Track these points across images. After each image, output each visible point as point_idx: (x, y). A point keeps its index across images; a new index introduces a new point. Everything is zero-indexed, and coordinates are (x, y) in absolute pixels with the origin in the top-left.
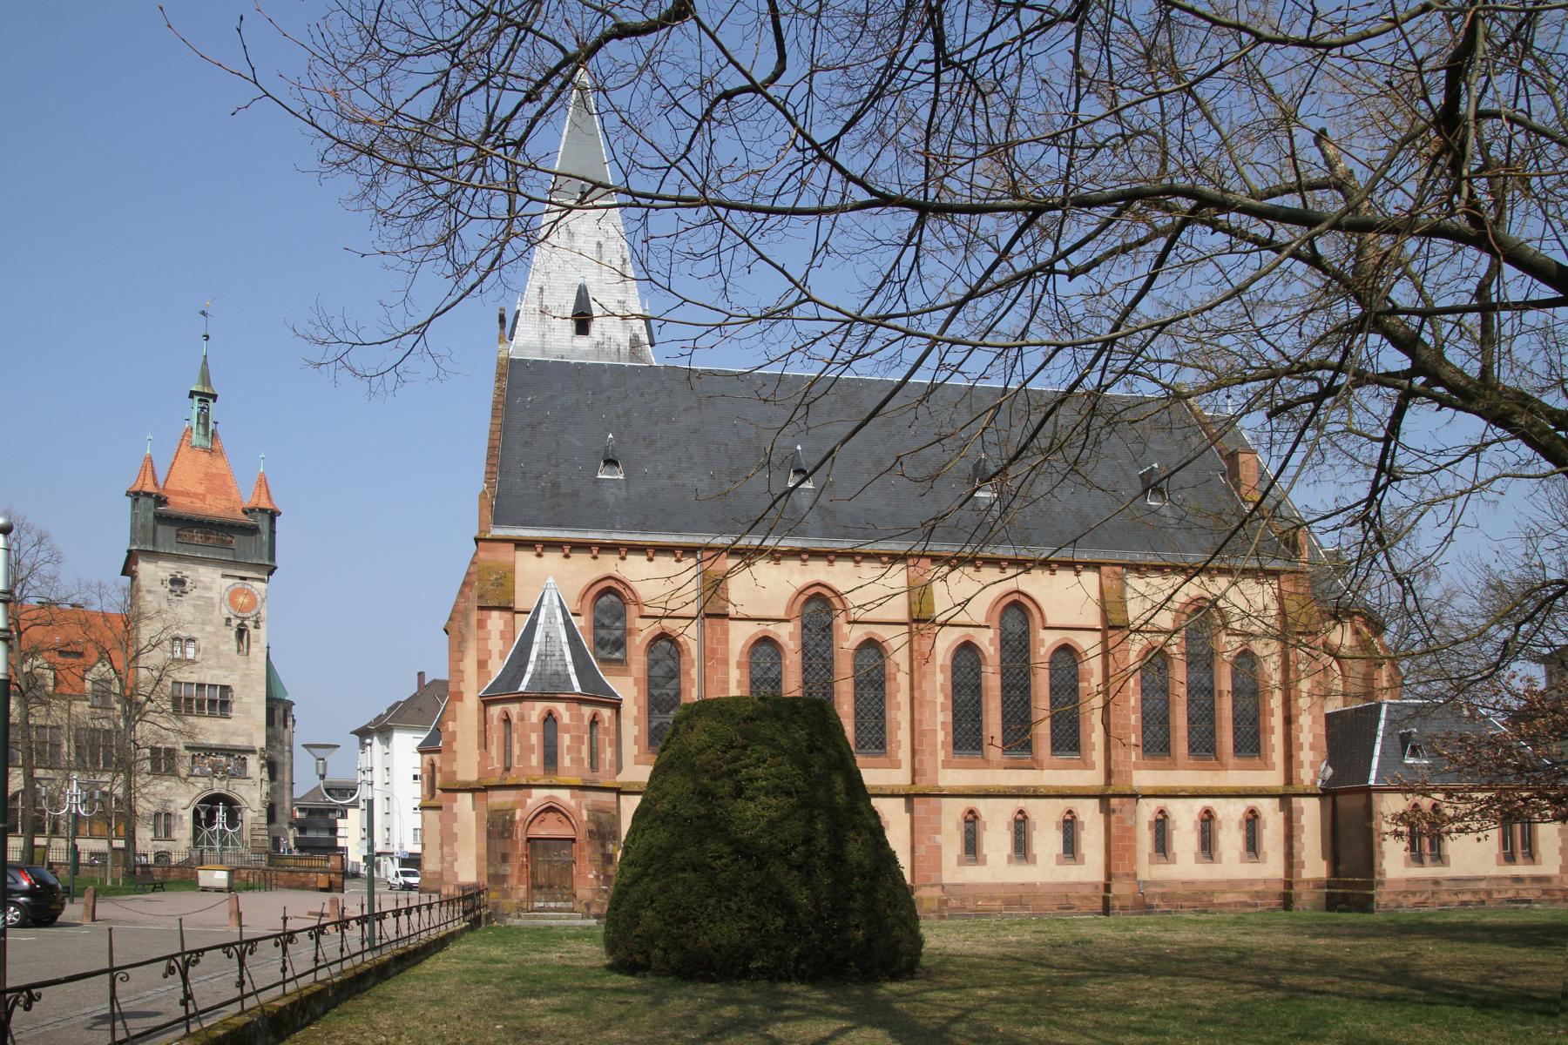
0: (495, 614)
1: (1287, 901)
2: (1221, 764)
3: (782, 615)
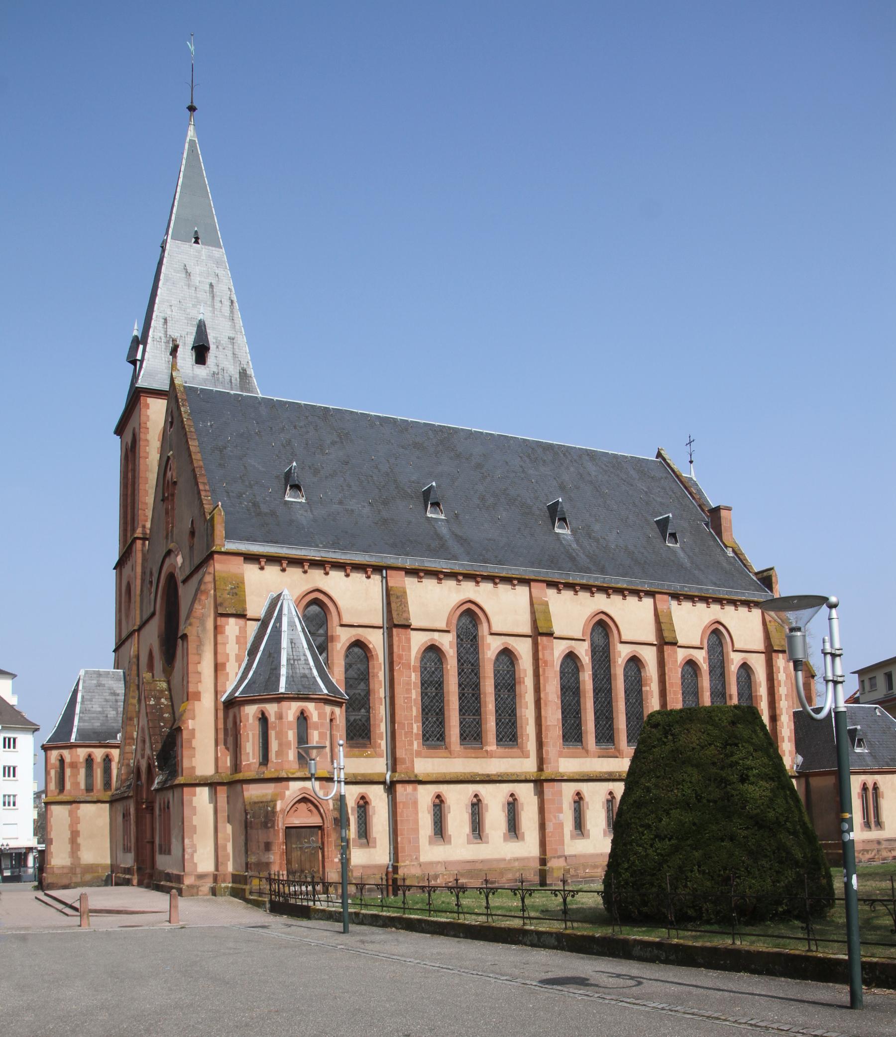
0: (232, 621)
3: (443, 626)
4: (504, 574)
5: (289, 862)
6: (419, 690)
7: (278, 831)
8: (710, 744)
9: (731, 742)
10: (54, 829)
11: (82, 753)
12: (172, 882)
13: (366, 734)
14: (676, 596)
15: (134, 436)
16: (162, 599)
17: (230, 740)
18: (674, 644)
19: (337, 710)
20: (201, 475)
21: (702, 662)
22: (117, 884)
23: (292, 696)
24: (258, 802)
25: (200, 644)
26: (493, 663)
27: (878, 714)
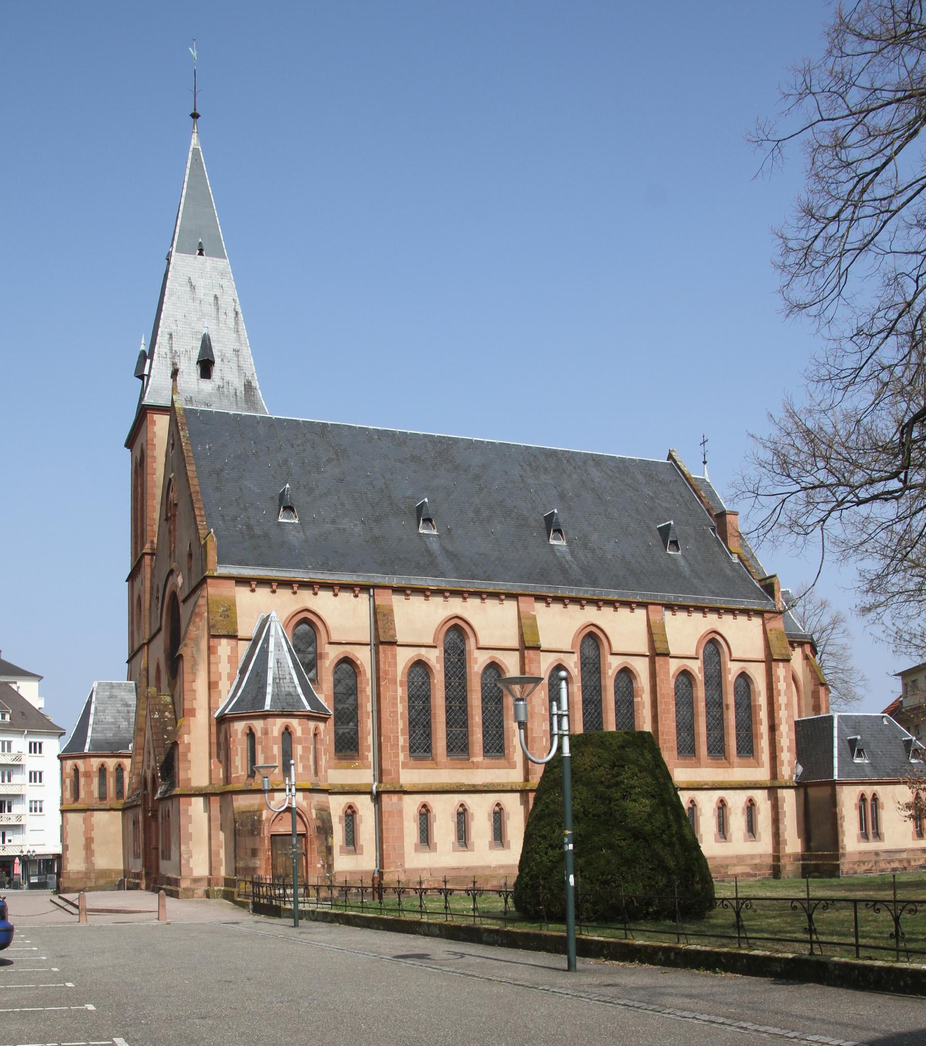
0: (224, 641)
1: (776, 871)
2: (729, 763)
3: (430, 641)
4: (491, 590)
5: (274, 867)
6: (407, 704)
7: (264, 838)
8: (600, 766)
9: (618, 764)
10: (69, 835)
11: (95, 763)
12: (171, 885)
13: (355, 747)
14: (670, 607)
15: (142, 451)
16: (167, 615)
17: (222, 753)
18: (667, 655)
19: (321, 726)
20: (198, 500)
21: (697, 672)
22: (129, 889)
23: (276, 713)
25: (195, 664)
26: (480, 676)
27: (885, 723)
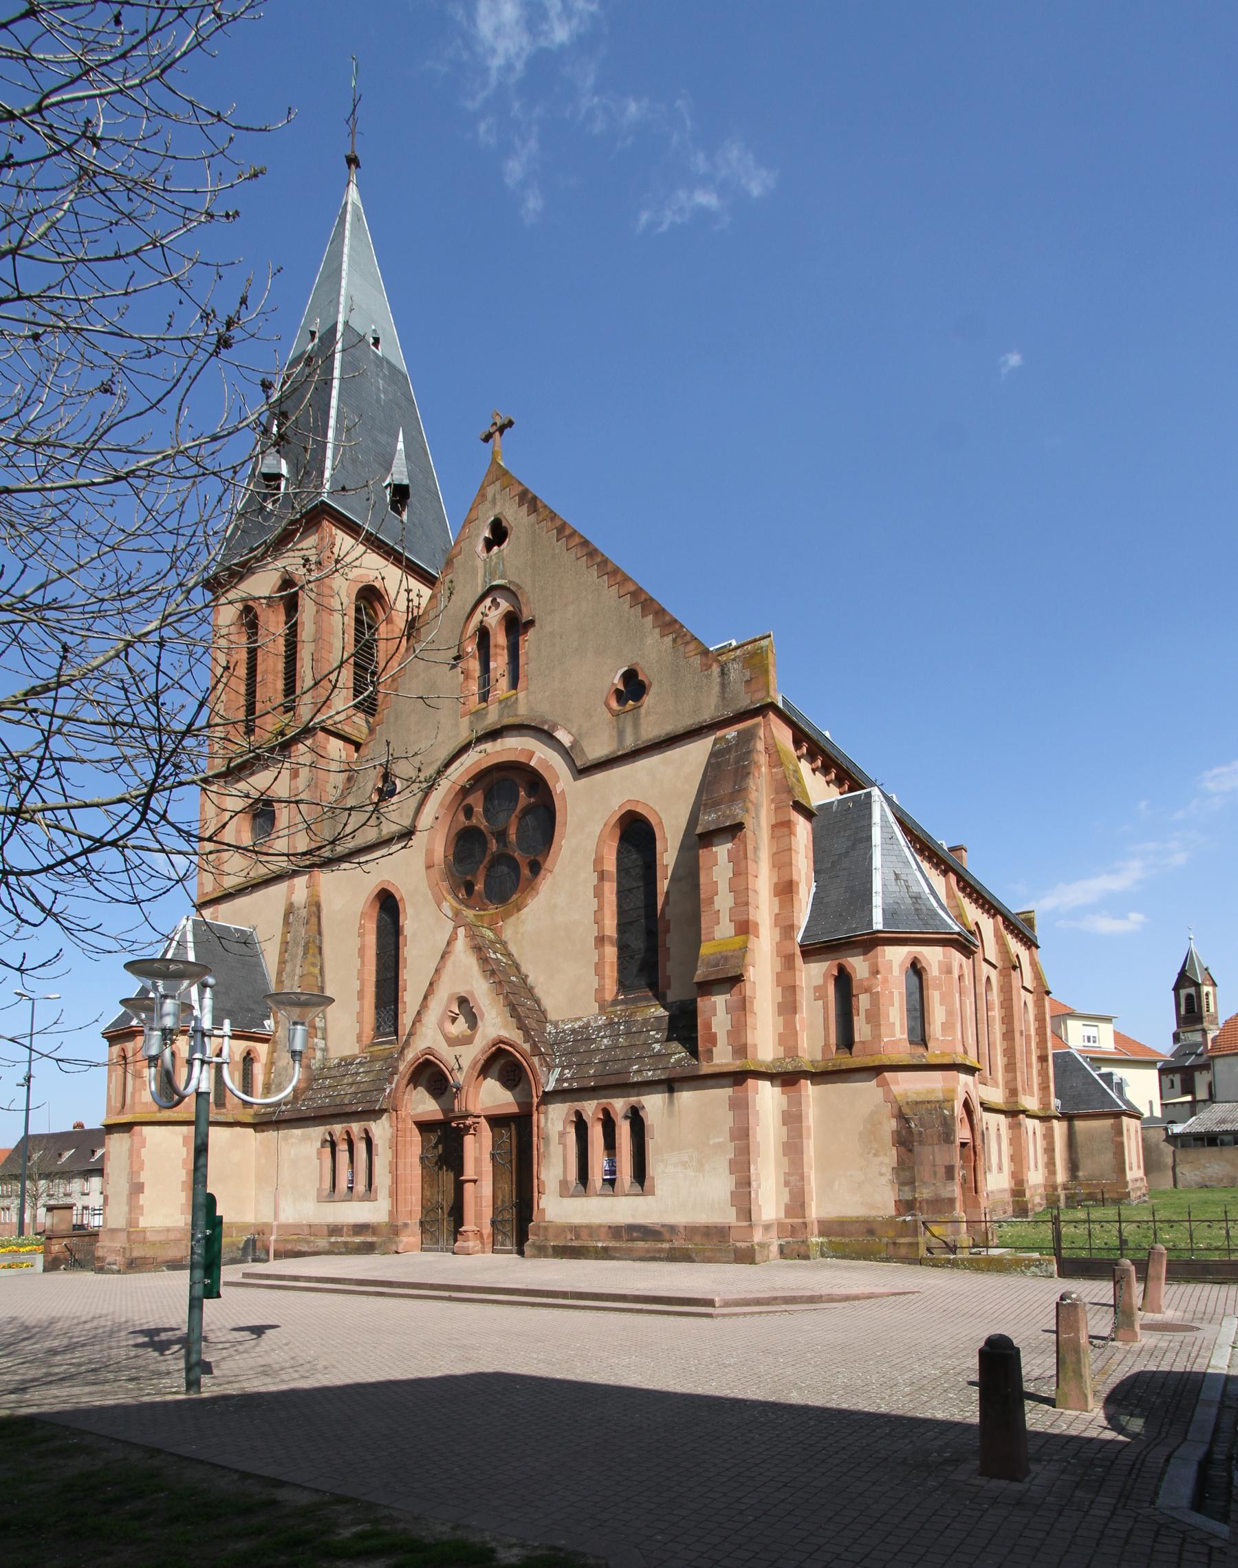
24: (923, 1102)
